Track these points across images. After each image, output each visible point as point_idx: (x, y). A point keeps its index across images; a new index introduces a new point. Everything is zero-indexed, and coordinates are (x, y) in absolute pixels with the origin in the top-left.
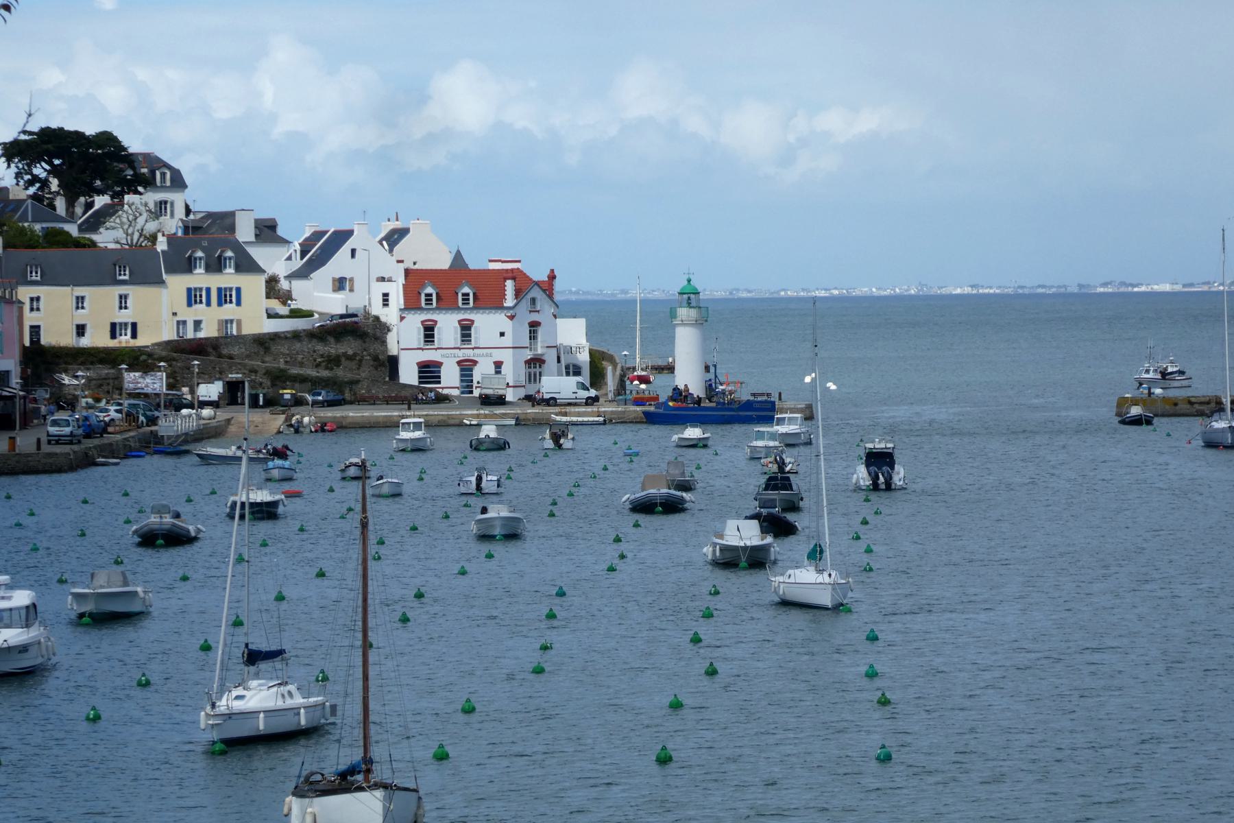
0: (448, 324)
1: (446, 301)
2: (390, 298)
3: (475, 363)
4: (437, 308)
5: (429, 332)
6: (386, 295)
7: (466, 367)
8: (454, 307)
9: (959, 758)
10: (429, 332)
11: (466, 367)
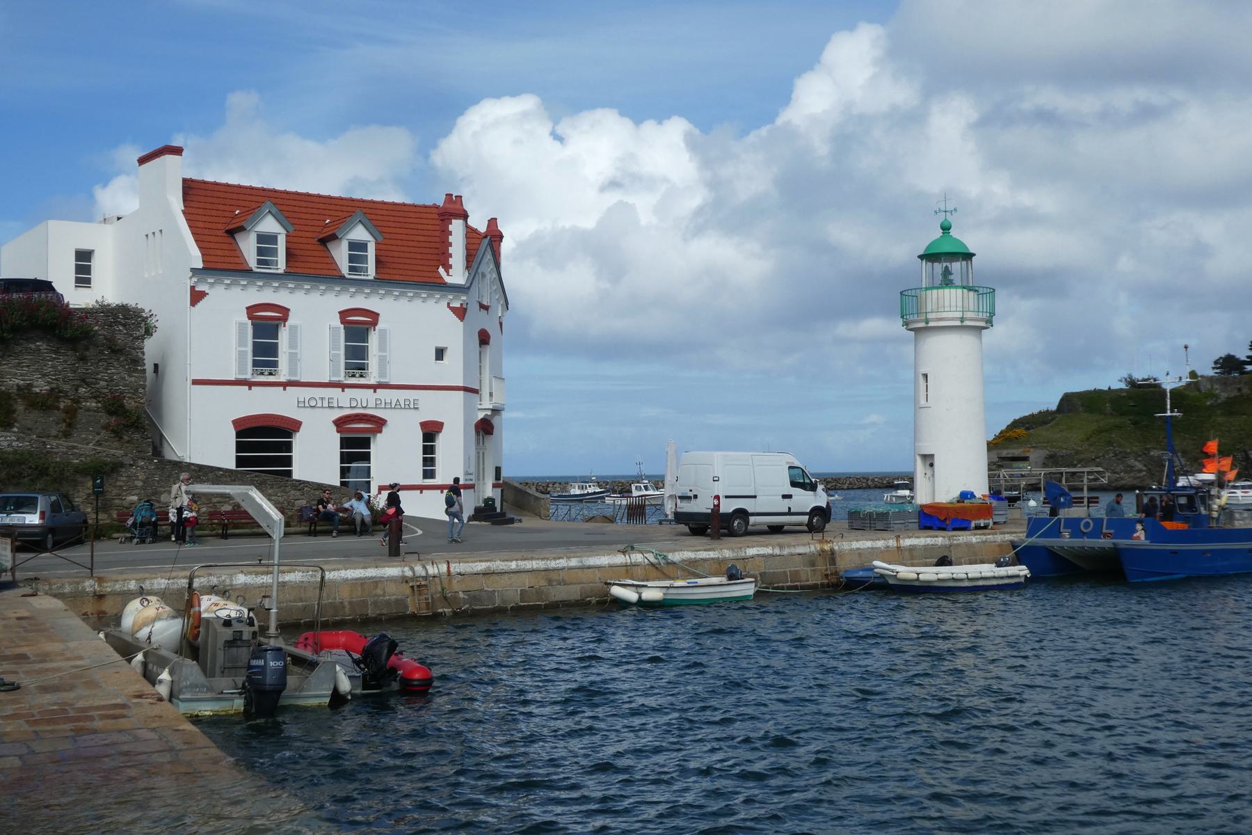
0: (314, 316)
1: (309, 261)
2: (96, 264)
3: (379, 423)
4: (287, 274)
5: (266, 327)
6: (84, 257)
7: (356, 442)
8: (327, 276)
9: (1003, 747)
10: (266, 327)
11: (356, 442)
